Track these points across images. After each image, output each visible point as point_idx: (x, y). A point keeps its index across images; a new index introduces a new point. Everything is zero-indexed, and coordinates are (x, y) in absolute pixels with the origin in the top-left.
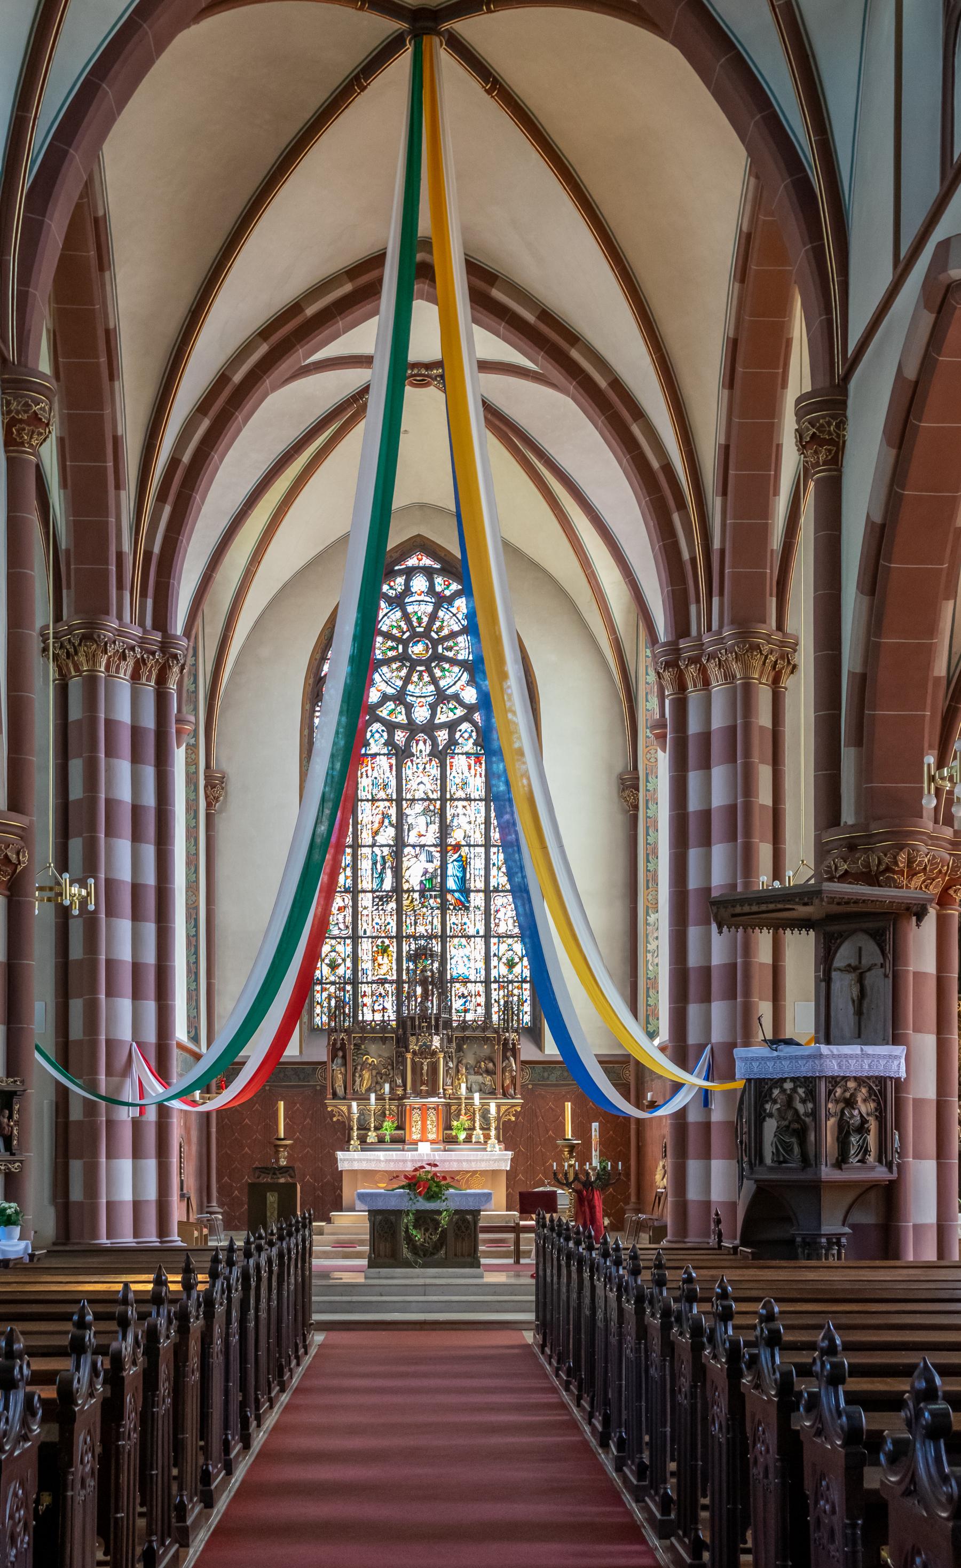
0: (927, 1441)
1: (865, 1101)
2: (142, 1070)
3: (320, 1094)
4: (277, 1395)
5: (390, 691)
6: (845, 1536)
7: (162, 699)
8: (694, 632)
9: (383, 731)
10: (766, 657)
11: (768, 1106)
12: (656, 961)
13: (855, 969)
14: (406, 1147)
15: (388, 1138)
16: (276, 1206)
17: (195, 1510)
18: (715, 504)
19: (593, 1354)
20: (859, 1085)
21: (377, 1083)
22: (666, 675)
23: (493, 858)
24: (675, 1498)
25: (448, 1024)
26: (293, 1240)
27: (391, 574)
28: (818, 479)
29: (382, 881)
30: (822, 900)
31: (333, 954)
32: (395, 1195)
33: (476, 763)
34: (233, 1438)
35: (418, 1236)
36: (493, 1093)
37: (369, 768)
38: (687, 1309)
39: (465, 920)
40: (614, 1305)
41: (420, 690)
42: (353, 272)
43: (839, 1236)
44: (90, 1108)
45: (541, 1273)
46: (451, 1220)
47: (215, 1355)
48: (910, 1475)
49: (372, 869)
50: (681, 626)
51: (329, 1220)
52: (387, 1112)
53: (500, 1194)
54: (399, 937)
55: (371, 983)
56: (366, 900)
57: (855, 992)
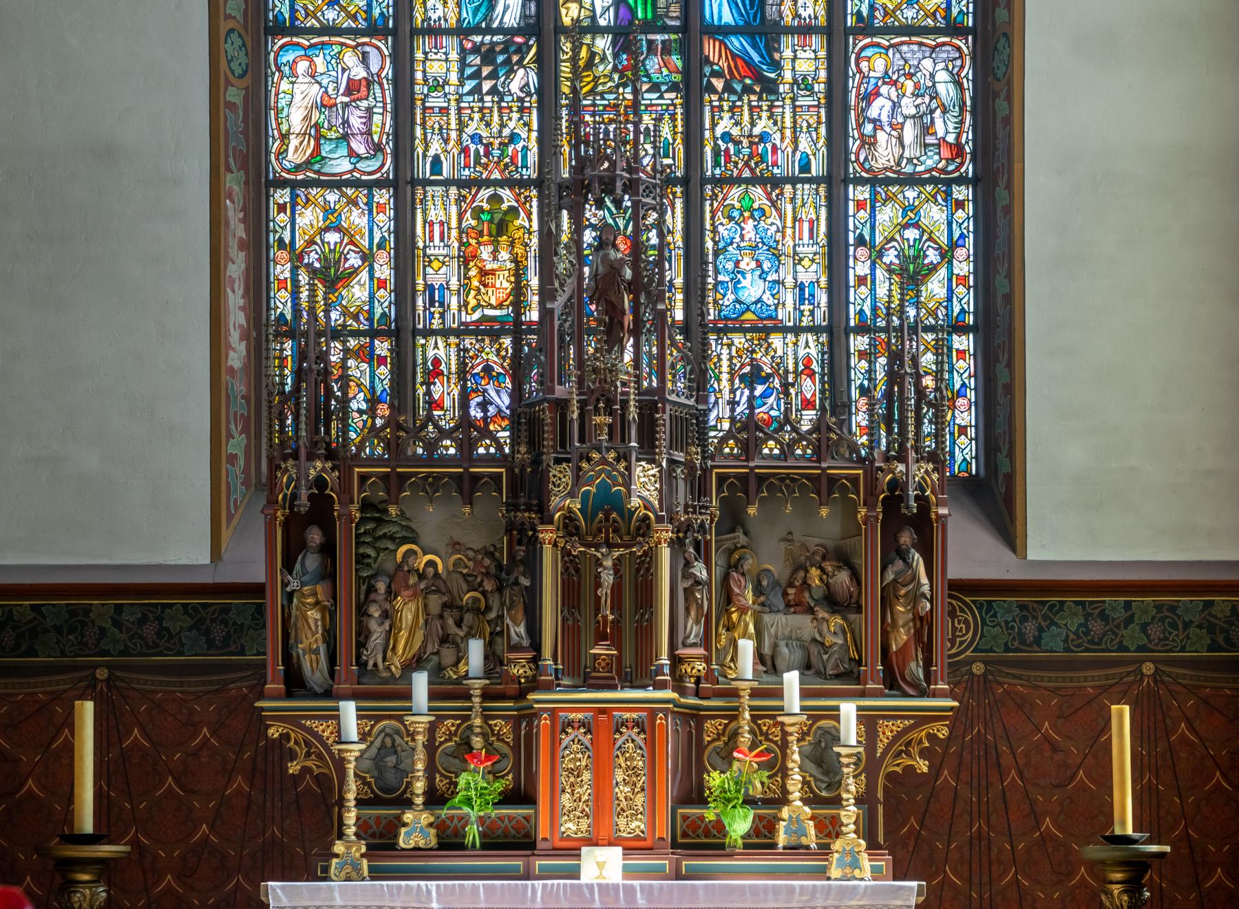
14: (539, 863)
15: (473, 832)
21: (445, 640)
52: (477, 742)
55: (458, 333)
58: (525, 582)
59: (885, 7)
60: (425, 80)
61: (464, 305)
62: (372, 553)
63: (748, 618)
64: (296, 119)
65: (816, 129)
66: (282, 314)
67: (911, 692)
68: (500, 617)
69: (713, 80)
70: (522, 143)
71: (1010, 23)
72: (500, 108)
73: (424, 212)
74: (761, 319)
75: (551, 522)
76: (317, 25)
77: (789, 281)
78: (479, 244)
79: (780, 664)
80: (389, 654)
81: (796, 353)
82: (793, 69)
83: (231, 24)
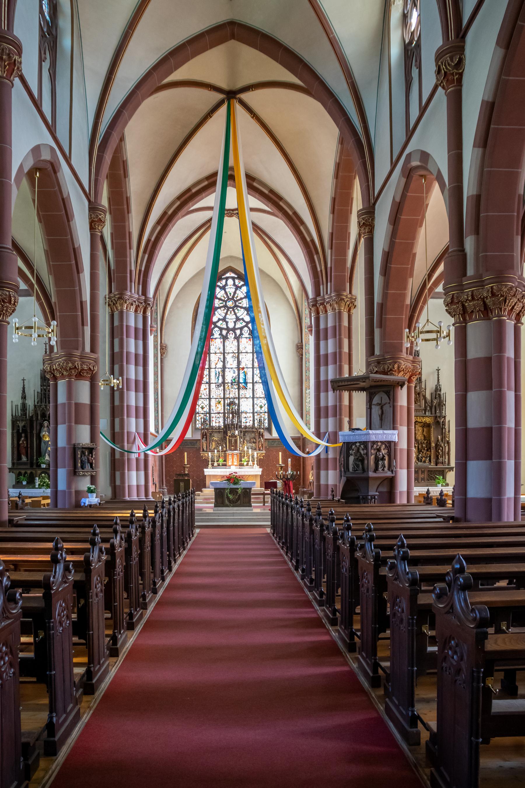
0: (460, 592)
1: (384, 449)
2: (139, 442)
3: (199, 450)
4: (182, 551)
6: (409, 623)
7: (145, 318)
8: (322, 294)
10: (346, 303)
11: (351, 452)
12: (309, 405)
13: (380, 404)
15: (221, 464)
16: (183, 486)
17: (149, 596)
18: (328, 252)
19: (292, 538)
20: (382, 444)
22: (313, 309)
23: (255, 372)
24: (325, 592)
25: (240, 427)
26: (188, 498)
27: (220, 279)
28: (366, 238)
30: (370, 380)
31: (202, 404)
32: (223, 483)
34: (165, 568)
35: (231, 497)
36: (255, 449)
37: (214, 343)
38: (331, 524)
39: (246, 392)
40: (301, 522)
41: (231, 317)
42: (208, 178)
43: (375, 496)
44: (122, 455)
45: (273, 509)
46: (242, 491)
47: (157, 540)
48: (450, 605)
50: (317, 293)
51: (202, 491)
53: (258, 482)
54: (224, 398)
56: (213, 386)
57: (380, 412)
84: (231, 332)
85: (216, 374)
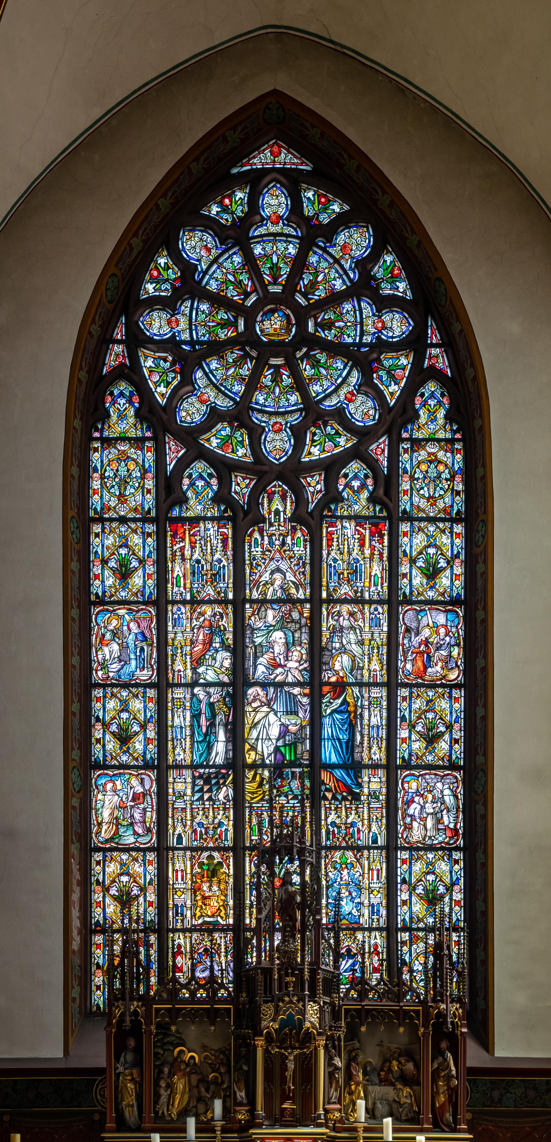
5: (223, 403)
9: (210, 475)
21: (199, 1099)
29: (209, 748)
33: (372, 535)
49: (192, 726)
58: (245, 1068)
59: (417, 754)
60: (174, 793)
61: (193, 915)
62: (161, 1052)
63: (360, 1088)
64: (106, 814)
65: (381, 820)
66: (98, 921)
67: (446, 1129)
68: (229, 1087)
69: (326, 793)
70: (225, 827)
71: (486, 764)
72: (213, 808)
73: (173, 864)
74: (351, 923)
75: (261, 1035)
76: (117, 764)
77: (366, 902)
78: (202, 882)
79: (378, 1114)
80: (170, 1107)
81: (369, 942)
82: (369, 788)
83: (74, 764)
84: (277, 486)
85: (196, 716)
